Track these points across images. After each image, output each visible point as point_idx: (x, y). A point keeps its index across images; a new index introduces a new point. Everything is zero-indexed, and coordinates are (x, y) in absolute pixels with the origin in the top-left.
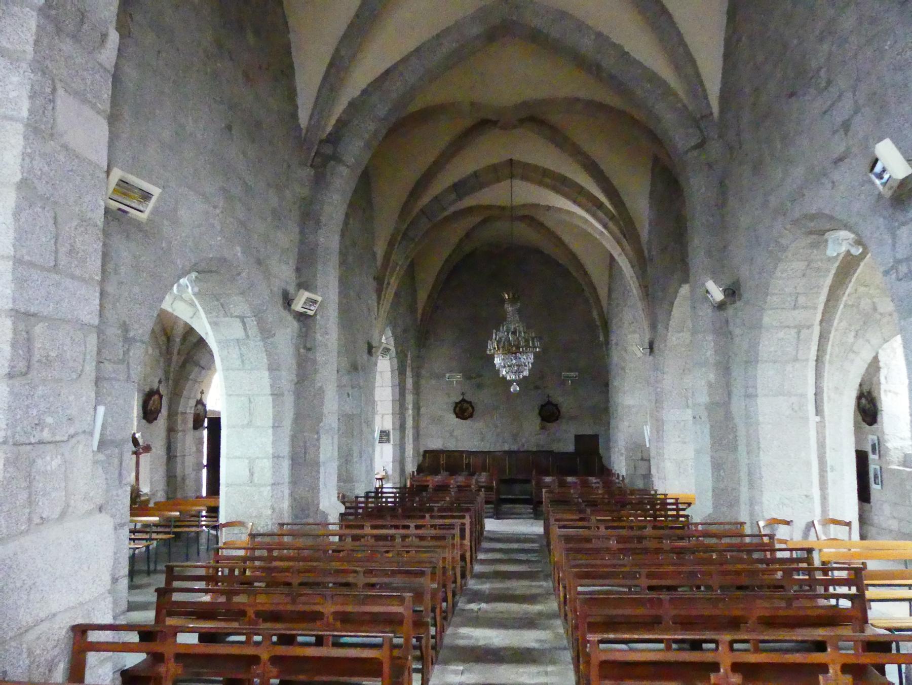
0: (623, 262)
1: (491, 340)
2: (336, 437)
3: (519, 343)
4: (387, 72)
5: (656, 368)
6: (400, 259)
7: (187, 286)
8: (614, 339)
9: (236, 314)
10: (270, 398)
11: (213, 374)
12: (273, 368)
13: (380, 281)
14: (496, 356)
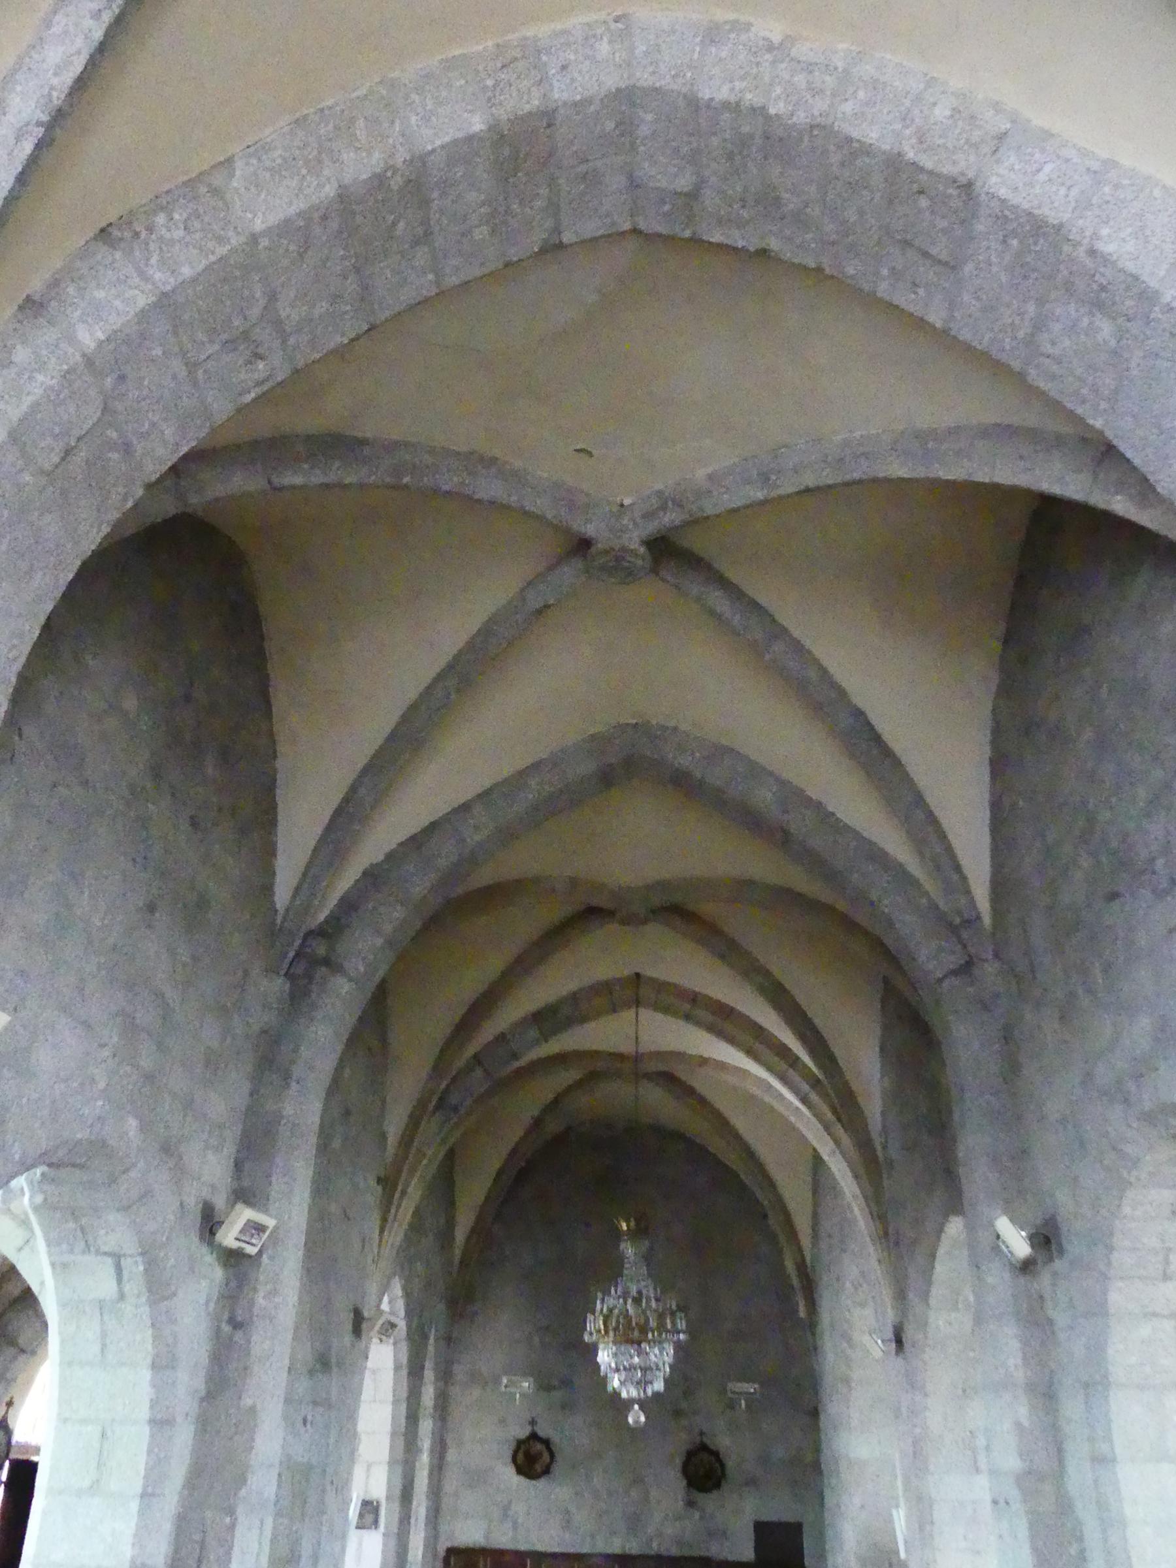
0: (838, 1168)
1: (594, 1313)
2: (269, 1522)
3: (647, 1320)
4: (433, 826)
5: (912, 1383)
6: (431, 1156)
7: (22, 1190)
8: (825, 1318)
9: (106, 1249)
10: (146, 1430)
11: (40, 1364)
12: (163, 1364)
13: (389, 1184)
14: (601, 1346)
